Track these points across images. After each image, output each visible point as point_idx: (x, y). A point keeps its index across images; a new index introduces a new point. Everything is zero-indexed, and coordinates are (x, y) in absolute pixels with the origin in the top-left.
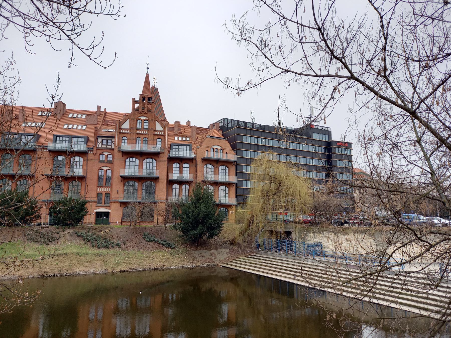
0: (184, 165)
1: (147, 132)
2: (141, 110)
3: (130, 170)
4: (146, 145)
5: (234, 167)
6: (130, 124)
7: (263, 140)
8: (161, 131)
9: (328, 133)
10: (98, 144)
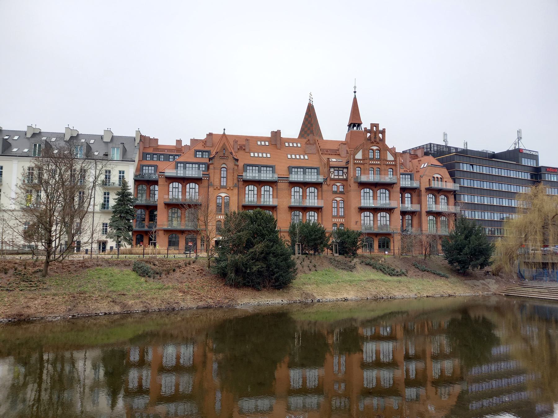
0: (406, 195)
1: (379, 162)
2: (373, 140)
3: (365, 201)
4: (379, 176)
5: (453, 196)
6: (363, 155)
7: (497, 170)
8: (392, 161)
9: (535, 157)
10: (331, 174)
